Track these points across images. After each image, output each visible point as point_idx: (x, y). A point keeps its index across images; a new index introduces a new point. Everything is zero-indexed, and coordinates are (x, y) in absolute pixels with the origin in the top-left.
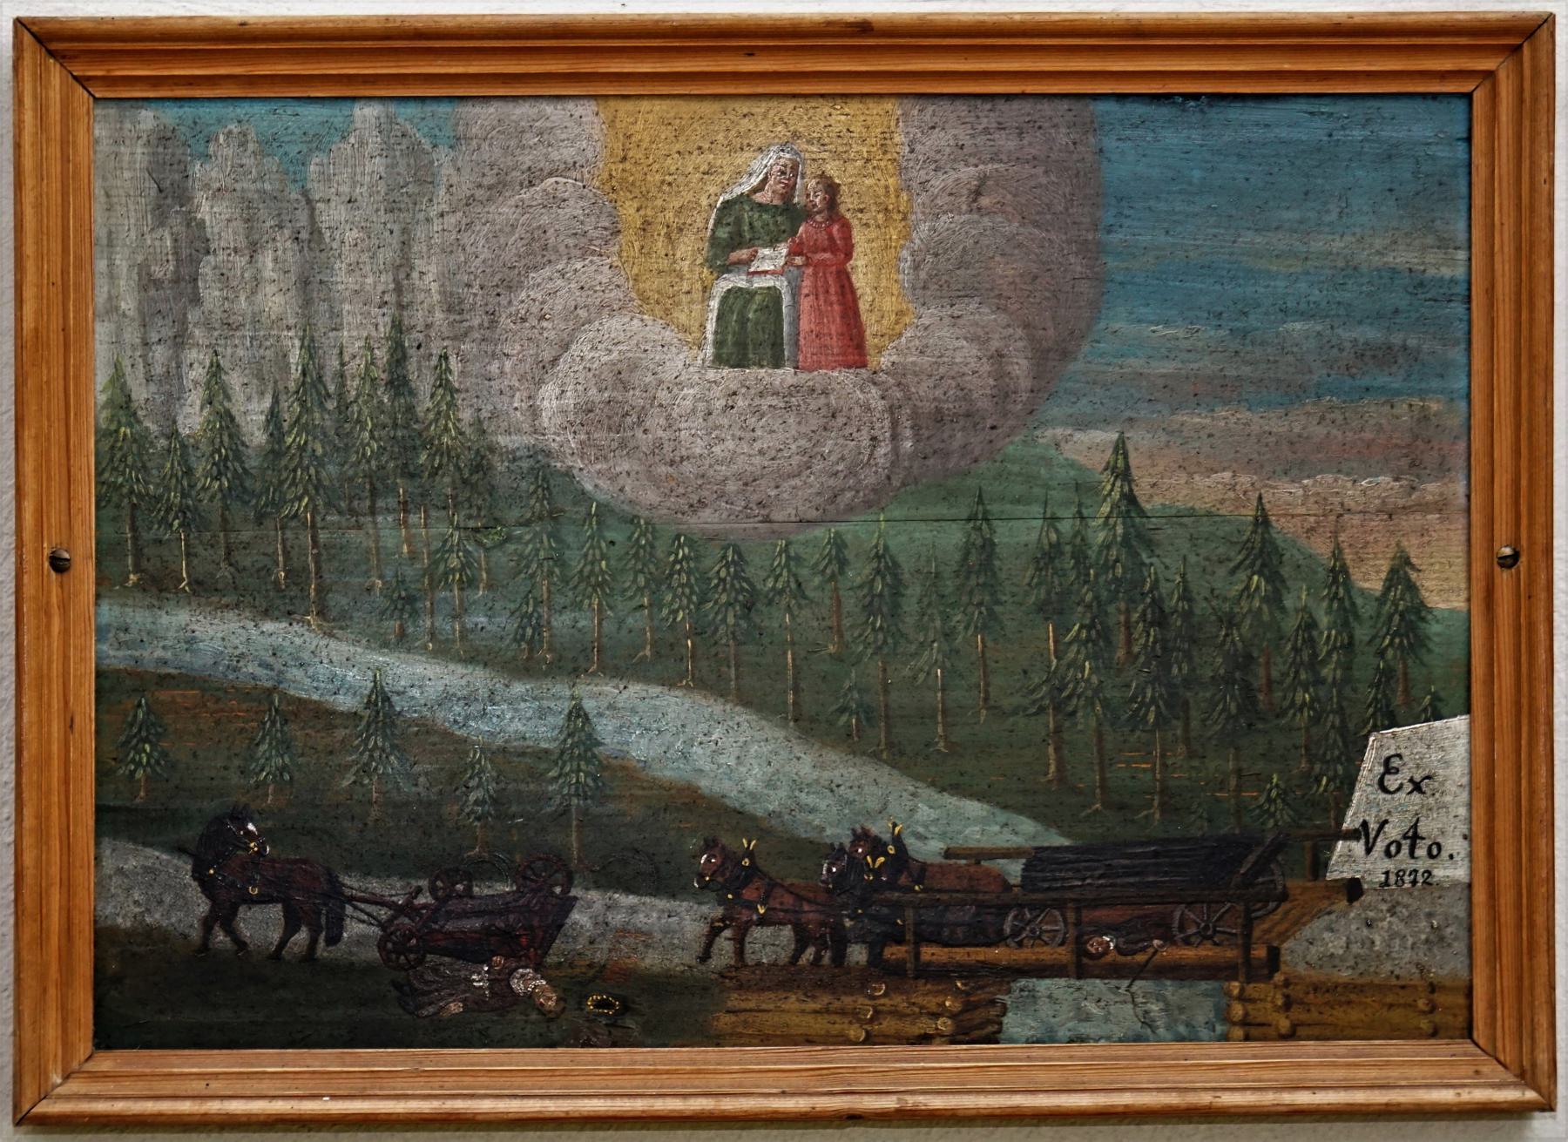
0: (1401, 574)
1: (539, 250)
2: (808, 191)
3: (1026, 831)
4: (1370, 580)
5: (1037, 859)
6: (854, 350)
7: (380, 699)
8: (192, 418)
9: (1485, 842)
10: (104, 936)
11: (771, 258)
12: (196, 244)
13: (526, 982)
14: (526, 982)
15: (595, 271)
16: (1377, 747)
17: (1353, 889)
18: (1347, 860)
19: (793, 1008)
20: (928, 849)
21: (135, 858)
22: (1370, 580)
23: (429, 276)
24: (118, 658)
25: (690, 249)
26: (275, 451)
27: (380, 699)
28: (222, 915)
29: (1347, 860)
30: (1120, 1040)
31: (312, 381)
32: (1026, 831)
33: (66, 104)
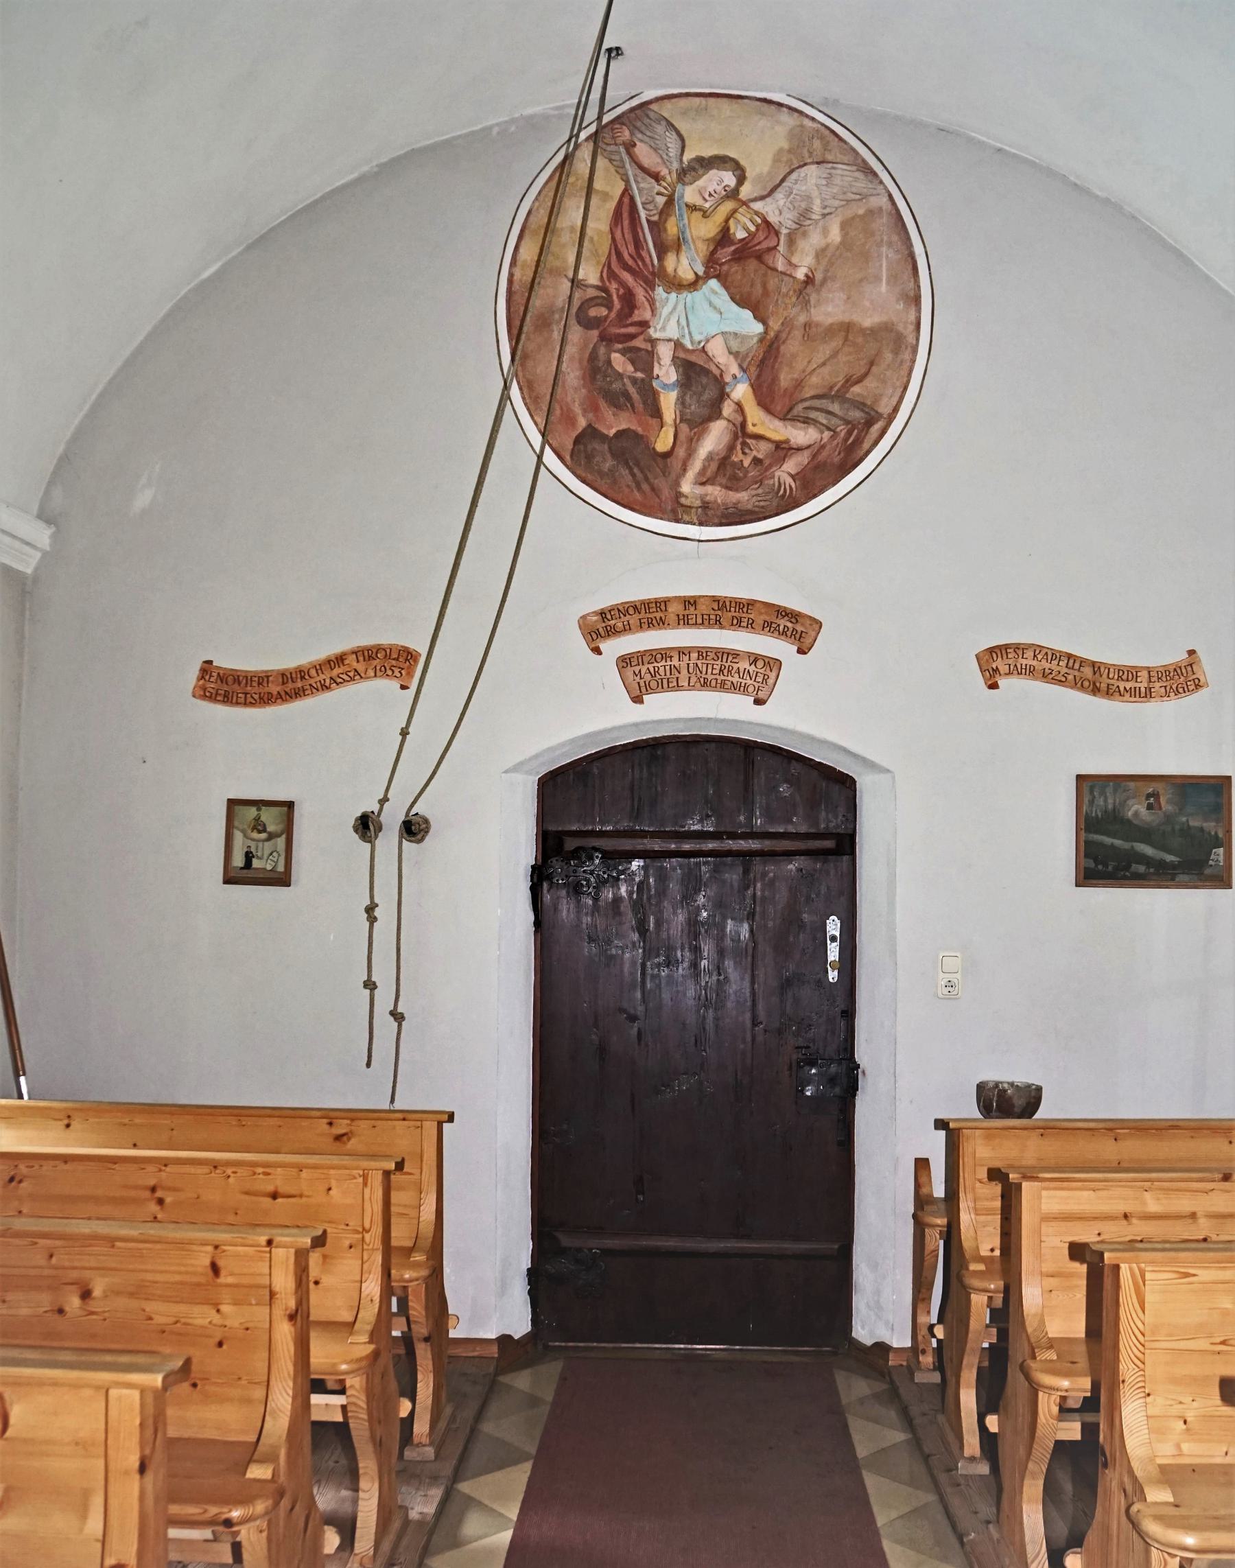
0: (1216, 833)
1: (1128, 798)
2: (1156, 792)
3: (1178, 859)
4: (1213, 833)
5: (1179, 862)
6: (1160, 808)
7: (1112, 844)
8: (1094, 815)
9: (1225, 861)
10: (1085, 868)
11: (1152, 799)
12: (1094, 797)
13: (1127, 874)
14: (1127, 874)
15: (1134, 800)
16: (1214, 851)
17: (1211, 866)
18: (1211, 862)
19: (1154, 877)
20: (1168, 861)
21: (1088, 860)
22: (1213, 833)
23: (1118, 800)
24: (1087, 866)
25: (1144, 798)
26: (1102, 818)
27: (1112, 844)
28: (1096, 866)
29: (1211, 862)
30: (958, 134)
31: (1106, 812)
32: (1178, 859)
33: (1033, 1562)
